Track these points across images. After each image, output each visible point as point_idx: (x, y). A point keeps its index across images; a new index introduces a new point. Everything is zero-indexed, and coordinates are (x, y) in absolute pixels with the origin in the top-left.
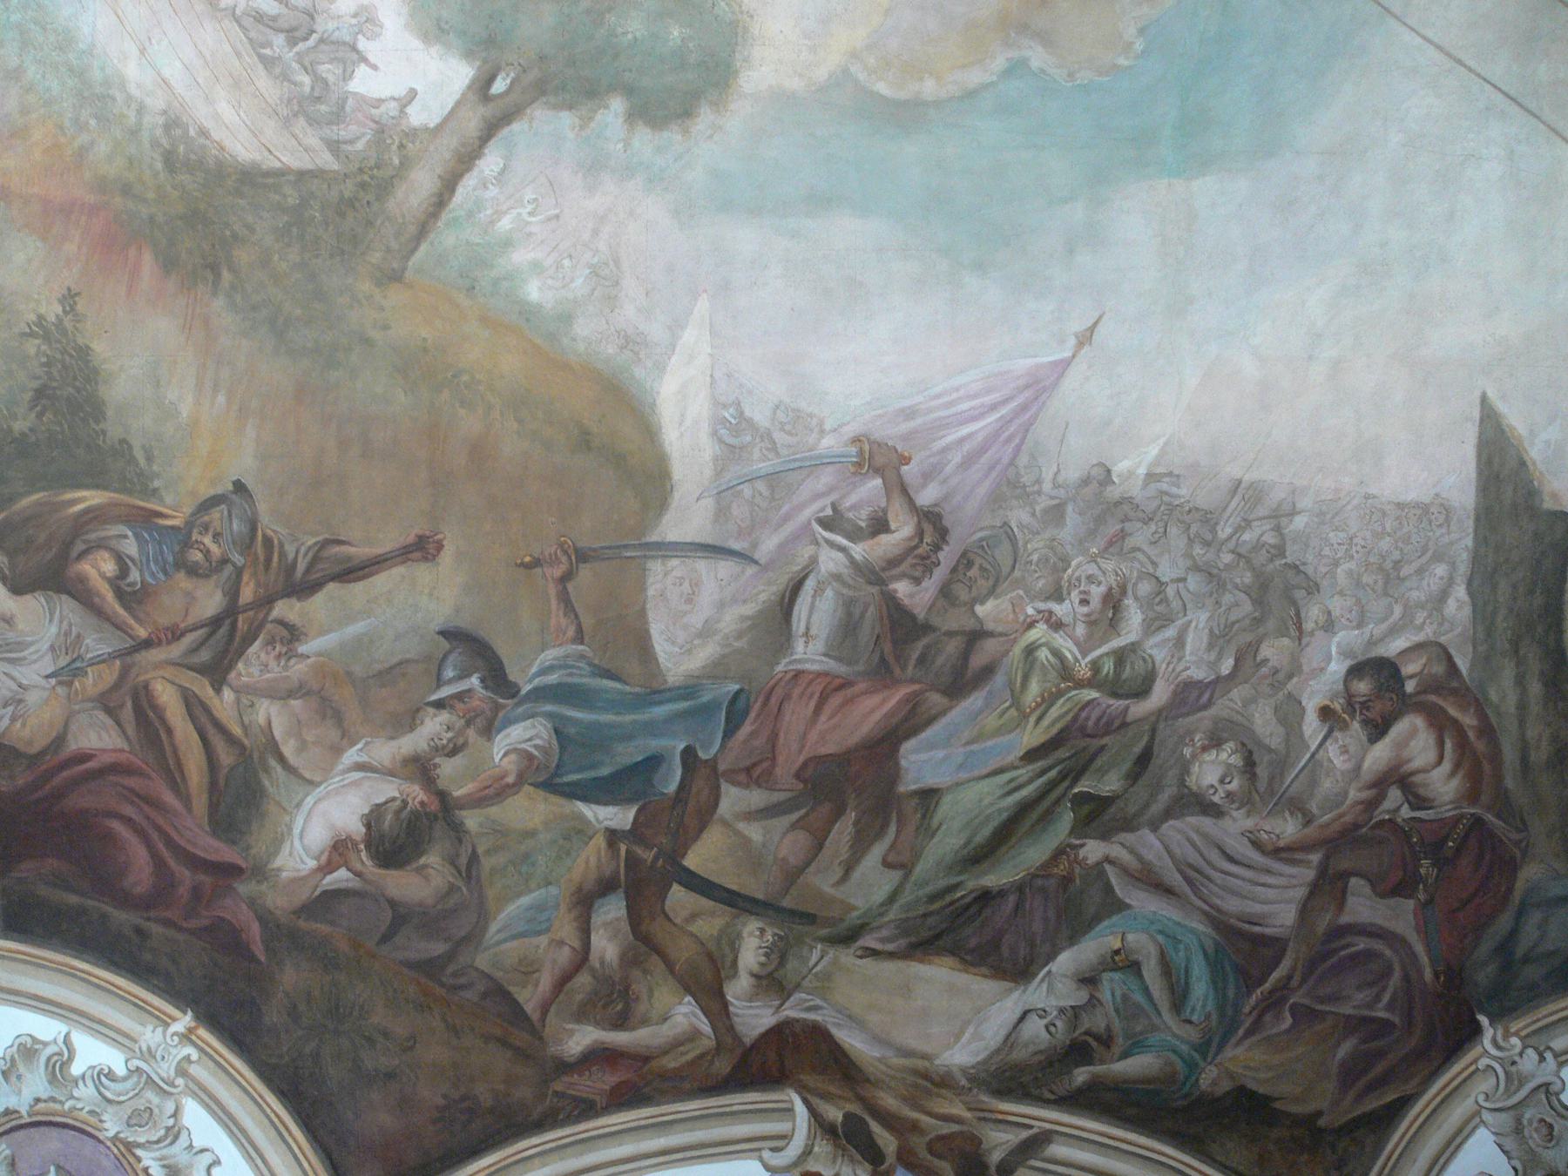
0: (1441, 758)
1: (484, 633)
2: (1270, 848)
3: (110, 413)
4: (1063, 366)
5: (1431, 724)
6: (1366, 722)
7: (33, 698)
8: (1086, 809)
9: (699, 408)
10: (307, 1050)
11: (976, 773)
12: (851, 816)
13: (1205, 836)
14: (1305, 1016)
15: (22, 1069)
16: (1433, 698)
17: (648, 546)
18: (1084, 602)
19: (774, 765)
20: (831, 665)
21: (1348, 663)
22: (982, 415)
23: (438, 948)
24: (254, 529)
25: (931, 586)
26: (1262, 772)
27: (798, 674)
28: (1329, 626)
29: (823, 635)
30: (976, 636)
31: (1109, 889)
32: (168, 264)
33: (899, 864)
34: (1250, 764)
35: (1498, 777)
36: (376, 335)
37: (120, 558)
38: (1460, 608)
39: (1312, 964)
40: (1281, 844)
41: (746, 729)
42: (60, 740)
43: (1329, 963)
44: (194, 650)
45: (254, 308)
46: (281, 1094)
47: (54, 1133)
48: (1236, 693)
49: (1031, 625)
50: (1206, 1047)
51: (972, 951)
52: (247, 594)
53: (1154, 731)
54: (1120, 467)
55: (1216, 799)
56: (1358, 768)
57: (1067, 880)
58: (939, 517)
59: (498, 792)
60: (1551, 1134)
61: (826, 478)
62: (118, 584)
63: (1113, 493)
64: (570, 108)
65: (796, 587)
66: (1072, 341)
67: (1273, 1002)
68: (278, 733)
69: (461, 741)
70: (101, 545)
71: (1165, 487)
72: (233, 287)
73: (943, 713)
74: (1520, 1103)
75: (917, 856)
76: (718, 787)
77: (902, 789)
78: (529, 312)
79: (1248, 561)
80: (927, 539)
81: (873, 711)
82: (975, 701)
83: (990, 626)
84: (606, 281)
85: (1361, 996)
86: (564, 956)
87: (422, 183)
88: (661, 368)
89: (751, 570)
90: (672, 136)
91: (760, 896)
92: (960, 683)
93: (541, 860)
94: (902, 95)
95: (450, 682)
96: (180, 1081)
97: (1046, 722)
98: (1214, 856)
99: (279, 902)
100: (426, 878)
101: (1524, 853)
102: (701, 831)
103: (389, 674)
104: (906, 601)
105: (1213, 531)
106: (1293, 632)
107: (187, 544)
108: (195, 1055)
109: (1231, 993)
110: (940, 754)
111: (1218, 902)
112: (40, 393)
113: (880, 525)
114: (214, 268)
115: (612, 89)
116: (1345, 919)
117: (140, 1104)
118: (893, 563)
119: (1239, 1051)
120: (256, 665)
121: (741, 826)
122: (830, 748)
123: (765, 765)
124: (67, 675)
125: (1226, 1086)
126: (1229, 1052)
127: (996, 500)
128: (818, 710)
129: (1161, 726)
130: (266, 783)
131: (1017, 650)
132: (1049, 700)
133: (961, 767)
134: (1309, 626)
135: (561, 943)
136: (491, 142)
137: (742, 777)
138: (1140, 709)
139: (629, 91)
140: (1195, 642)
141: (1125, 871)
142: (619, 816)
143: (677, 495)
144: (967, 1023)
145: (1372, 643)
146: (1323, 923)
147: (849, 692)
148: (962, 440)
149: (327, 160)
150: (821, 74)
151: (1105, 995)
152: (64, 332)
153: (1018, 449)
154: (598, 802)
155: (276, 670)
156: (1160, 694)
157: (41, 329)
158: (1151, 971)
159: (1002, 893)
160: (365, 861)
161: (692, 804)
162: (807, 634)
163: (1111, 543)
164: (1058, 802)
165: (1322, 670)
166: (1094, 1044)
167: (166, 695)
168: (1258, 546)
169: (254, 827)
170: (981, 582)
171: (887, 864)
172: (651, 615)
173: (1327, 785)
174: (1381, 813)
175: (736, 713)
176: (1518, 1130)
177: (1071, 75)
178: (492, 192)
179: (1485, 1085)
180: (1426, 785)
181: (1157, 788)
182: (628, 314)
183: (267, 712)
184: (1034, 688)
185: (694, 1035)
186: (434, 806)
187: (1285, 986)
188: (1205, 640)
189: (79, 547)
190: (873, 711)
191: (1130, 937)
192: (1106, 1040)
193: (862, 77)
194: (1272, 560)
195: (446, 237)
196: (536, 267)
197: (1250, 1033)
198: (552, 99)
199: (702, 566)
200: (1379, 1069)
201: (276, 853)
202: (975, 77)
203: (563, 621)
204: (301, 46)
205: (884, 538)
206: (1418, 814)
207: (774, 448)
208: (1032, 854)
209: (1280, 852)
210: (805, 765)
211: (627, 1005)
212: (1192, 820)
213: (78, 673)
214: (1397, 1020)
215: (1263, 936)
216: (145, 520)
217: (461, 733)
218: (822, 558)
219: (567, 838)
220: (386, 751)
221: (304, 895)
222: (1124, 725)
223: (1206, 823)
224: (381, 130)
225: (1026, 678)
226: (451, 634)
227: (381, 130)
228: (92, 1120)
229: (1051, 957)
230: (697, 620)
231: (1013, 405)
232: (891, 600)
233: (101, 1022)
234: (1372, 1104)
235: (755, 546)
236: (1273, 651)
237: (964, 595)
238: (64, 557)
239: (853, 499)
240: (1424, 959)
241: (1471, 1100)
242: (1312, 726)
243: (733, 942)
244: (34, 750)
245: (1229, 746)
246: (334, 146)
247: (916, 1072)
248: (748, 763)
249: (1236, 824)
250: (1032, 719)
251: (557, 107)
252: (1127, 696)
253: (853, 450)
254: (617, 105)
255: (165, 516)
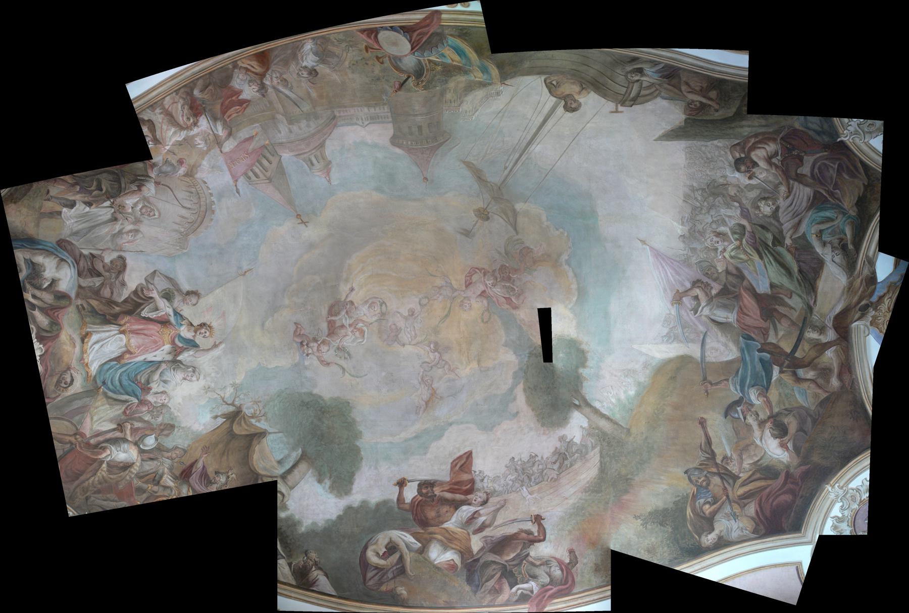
0: (763, 148)
1: (726, 406)
2: (788, 194)
3: (666, 507)
4: (652, 248)
5: (754, 150)
6: (753, 167)
7: (741, 525)
8: (776, 243)
9: (663, 347)
10: (837, 454)
11: (766, 272)
12: (777, 307)
13: (785, 211)
14: (836, 186)
15: (840, 529)
16: (746, 150)
17: (702, 361)
18: (718, 242)
19: (763, 328)
20: (735, 311)
21: (736, 172)
22: (665, 270)
23: (809, 419)
24: (697, 468)
25: (713, 284)
26: (766, 195)
27: (737, 321)
28: (725, 177)
29: (726, 314)
30: (727, 272)
31: (799, 237)
32: (626, 492)
33: (791, 295)
34: (764, 199)
35: (769, 133)
36: (644, 436)
37: (705, 504)
38: (720, 142)
39: (822, 184)
40: (787, 191)
41: (753, 335)
42: (752, 518)
43: (822, 180)
44: (729, 484)
45: (638, 469)
46: (848, 462)
47: (856, 521)
48: (744, 202)
49: (724, 257)
50: (844, 213)
51: (815, 275)
52: (714, 470)
53: (755, 224)
54: (680, 232)
55: (774, 208)
56: (766, 170)
57: (796, 249)
58: (693, 282)
59: (768, 403)
60: (872, 124)
61: (683, 312)
62: (711, 504)
63: (687, 234)
64: (582, 383)
65: (714, 321)
66: (644, 246)
67: (832, 194)
68: (752, 462)
69: (755, 413)
70: (701, 509)
71: (685, 221)
72: (632, 475)
73: (749, 281)
74: (863, 132)
75: (788, 289)
76: (768, 343)
77: (770, 293)
78: (638, 394)
79: (706, 198)
80: (700, 285)
81: (748, 300)
82: (746, 273)
83: (725, 268)
84: (629, 373)
85: (831, 171)
86: (813, 386)
87: (603, 424)
88: (653, 358)
89: (709, 333)
90: (589, 355)
91: (798, 332)
92: (741, 276)
93: (787, 391)
94: (576, 293)
95: (739, 415)
96: (844, 488)
97: (751, 253)
98: (790, 209)
99: (796, 461)
100: (790, 422)
101: (792, 127)
102: (780, 348)
103: (737, 433)
104: (717, 291)
105: (698, 207)
106: (727, 186)
107: (701, 486)
108: (838, 484)
109: (829, 206)
110: (760, 282)
111: (803, 208)
112: (661, 525)
113: (696, 298)
114: (627, 480)
115: (577, 372)
116: (809, 174)
117: (850, 499)
118: (707, 294)
119: (845, 204)
120: (733, 468)
121: (779, 337)
122: (758, 312)
123: (762, 330)
124: (735, 517)
125: (855, 209)
126: (846, 207)
127: (689, 266)
128: (748, 315)
129: (753, 222)
130: (765, 465)
131: (732, 261)
132: (746, 252)
133: (764, 276)
134: (725, 182)
135: (809, 387)
136: (592, 404)
137: (766, 336)
138: (748, 228)
139: (577, 367)
140: (729, 212)
141: (794, 233)
142: (776, 370)
143: (687, 354)
144: (835, 277)
145: (730, 165)
146: (810, 181)
147: (743, 307)
148: (672, 275)
149: (597, 450)
150: (571, 315)
151: (829, 239)
152: (645, 519)
153: (674, 260)
154: (772, 376)
155: (735, 462)
156: (744, 222)
157: (644, 524)
158: (823, 227)
159: (799, 266)
160: (786, 438)
161: (773, 350)
162: (726, 318)
163: (701, 235)
164: (774, 250)
165: (738, 179)
166: (842, 243)
167: (741, 491)
168: (702, 195)
169: (776, 468)
170: (712, 270)
171: (791, 298)
172: (721, 361)
173: (771, 178)
174: (779, 164)
175: (748, 338)
176: (870, 133)
177: (570, 248)
178: (605, 404)
179: (857, 141)
180: (771, 152)
181: (771, 224)
182: (638, 367)
183: (746, 464)
184: (742, 256)
185: (836, 351)
186: (772, 420)
187: (828, 192)
188: (728, 210)
189: (702, 514)
190: (748, 300)
191: (813, 232)
192: (841, 240)
193: (572, 305)
194: (706, 192)
195: (617, 417)
196: (625, 392)
197: (840, 201)
198: (580, 388)
199: (707, 347)
200: (852, 168)
201: (783, 462)
202: (571, 274)
203: (723, 384)
204: (568, 457)
205: (700, 297)
206: (780, 154)
207: (675, 327)
208: (789, 258)
209: (790, 190)
210: (763, 319)
211: (827, 369)
212: (780, 215)
213: (735, 514)
214: (838, 162)
215: (813, 197)
216: (695, 497)
217: (752, 412)
218: (705, 314)
219: (781, 384)
220: (757, 433)
221: (794, 455)
222: (753, 232)
223: (781, 211)
224: (589, 435)
225: (739, 258)
226: (726, 415)
227: (589, 435)
228: (854, 511)
229: (817, 253)
230: (722, 348)
231: (662, 262)
232: (717, 295)
233: (828, 509)
234: (861, 170)
235: (702, 332)
236: (732, 191)
237: (716, 275)
238: (704, 518)
239: (689, 305)
240: (821, 154)
241: (862, 144)
242: (754, 182)
243: (810, 341)
244: (754, 525)
245: (759, 204)
246: (593, 448)
247: (848, 291)
248: (762, 335)
249: (781, 202)
250: (751, 257)
251: (582, 387)
252: (745, 231)
253: (675, 305)
254: (581, 370)
255: (694, 492)
